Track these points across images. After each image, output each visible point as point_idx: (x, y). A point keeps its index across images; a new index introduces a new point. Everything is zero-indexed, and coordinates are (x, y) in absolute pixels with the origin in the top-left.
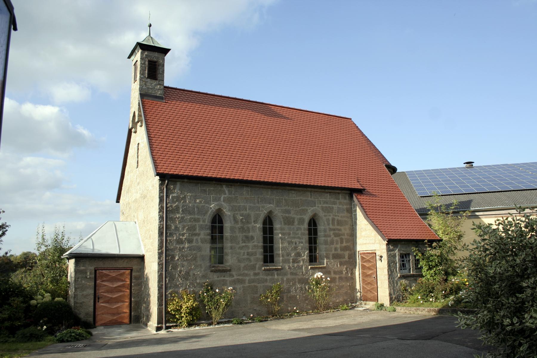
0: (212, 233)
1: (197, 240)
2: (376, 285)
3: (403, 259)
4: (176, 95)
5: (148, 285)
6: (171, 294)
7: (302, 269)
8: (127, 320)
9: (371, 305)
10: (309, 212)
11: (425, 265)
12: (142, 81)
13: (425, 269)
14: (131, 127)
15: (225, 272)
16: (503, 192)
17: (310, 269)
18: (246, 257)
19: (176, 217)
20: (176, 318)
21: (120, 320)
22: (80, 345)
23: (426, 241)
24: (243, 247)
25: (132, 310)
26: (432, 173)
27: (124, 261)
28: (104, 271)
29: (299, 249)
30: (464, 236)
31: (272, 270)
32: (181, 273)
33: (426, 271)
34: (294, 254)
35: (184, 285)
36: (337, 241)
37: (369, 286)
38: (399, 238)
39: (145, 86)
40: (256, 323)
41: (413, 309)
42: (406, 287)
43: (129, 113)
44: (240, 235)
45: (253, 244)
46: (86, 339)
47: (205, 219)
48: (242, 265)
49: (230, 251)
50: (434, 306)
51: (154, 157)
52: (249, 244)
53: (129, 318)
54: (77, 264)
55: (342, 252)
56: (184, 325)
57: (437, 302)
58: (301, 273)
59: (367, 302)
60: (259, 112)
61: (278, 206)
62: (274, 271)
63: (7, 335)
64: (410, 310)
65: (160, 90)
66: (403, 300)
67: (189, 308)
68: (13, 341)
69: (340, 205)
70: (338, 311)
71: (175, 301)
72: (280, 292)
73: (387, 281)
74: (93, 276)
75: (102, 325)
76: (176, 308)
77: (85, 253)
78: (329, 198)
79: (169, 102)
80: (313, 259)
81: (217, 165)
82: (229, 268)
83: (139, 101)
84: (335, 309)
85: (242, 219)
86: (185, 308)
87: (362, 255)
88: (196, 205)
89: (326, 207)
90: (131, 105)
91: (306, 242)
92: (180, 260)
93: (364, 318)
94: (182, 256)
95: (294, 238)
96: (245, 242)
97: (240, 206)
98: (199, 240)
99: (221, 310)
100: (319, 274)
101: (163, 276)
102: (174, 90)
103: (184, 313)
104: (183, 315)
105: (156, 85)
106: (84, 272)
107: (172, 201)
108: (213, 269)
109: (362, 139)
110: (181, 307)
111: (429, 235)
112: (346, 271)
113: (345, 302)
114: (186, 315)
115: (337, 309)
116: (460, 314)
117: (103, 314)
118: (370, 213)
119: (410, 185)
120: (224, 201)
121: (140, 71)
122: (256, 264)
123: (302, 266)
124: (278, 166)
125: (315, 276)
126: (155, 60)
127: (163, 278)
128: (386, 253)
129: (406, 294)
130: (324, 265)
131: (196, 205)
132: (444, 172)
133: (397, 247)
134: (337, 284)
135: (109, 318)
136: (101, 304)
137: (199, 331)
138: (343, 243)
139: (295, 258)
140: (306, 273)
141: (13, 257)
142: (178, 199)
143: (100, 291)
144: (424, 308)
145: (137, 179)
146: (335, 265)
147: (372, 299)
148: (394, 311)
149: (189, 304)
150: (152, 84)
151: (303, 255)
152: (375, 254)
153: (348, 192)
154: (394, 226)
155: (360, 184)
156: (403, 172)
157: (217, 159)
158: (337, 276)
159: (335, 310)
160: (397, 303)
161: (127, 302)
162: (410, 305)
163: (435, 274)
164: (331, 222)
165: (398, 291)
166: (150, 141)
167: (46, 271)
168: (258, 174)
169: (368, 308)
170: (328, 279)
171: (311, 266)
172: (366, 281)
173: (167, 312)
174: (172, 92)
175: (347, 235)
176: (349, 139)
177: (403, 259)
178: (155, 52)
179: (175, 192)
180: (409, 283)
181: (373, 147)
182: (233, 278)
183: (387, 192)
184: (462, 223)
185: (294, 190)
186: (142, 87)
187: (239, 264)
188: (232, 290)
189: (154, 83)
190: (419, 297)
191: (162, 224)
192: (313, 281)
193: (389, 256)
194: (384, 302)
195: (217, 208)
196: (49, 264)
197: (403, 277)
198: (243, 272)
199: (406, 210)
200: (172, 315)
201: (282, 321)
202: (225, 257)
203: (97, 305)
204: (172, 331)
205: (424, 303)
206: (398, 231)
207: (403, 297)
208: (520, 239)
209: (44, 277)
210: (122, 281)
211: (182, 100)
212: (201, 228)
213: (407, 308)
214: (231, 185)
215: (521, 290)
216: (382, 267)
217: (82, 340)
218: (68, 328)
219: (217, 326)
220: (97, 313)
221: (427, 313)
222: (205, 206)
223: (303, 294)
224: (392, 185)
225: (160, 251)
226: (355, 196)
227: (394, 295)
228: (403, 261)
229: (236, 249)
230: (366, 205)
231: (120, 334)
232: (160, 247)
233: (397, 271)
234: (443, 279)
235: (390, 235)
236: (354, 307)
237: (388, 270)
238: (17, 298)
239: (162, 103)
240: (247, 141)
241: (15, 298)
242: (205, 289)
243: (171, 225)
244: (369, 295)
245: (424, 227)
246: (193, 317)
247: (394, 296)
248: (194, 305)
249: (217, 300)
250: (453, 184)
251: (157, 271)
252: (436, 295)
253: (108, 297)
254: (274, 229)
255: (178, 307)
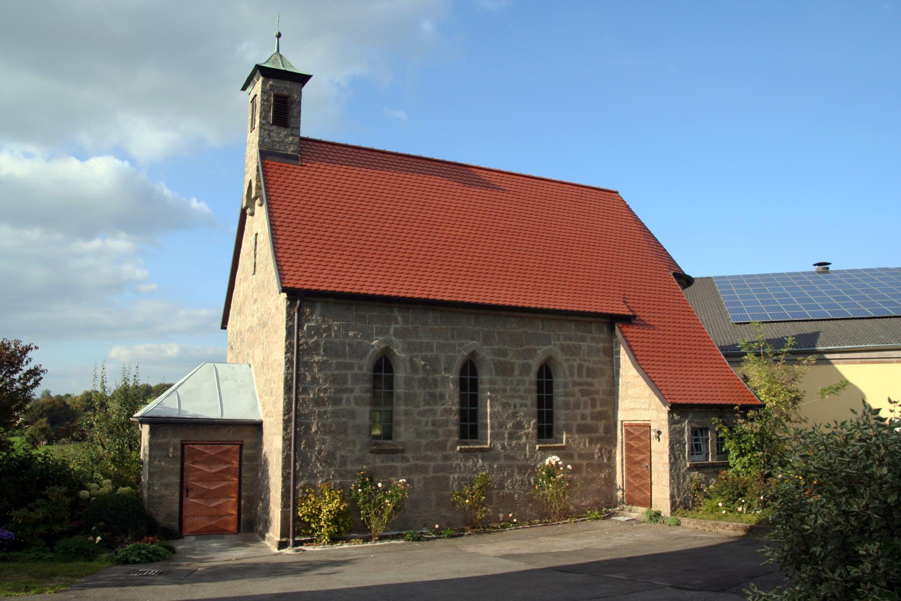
0: (374, 388)
1: (348, 400)
2: (649, 480)
3: (696, 437)
4: (320, 152)
5: (267, 471)
6: (304, 488)
7: (525, 450)
8: (233, 527)
9: (639, 512)
10: (538, 354)
11: (734, 448)
12: (264, 129)
13: (733, 454)
14: (244, 205)
15: (394, 453)
16: (877, 319)
17: (539, 450)
18: (429, 428)
19: (314, 362)
20: (312, 528)
21: (222, 527)
22: (151, 570)
23: (737, 407)
24: (426, 411)
25: (242, 510)
26: (757, 280)
27: (229, 431)
28: (197, 447)
29: (520, 416)
30: (804, 398)
31: (474, 452)
32: (321, 453)
33: (735, 458)
34: (511, 424)
35: (326, 474)
36: (586, 403)
37: (638, 481)
38: (690, 402)
39: (268, 137)
40: (443, 540)
41: (709, 523)
42: (700, 484)
43: (244, 182)
44: (421, 393)
45: (443, 407)
46: (165, 559)
47: (363, 365)
48: (424, 442)
49: (403, 418)
50: (745, 520)
51: (279, 259)
52: (436, 408)
53: (236, 523)
54: (152, 432)
55: (594, 422)
56: (324, 540)
57: (750, 513)
58: (523, 457)
59: (634, 508)
60: (459, 181)
61: (486, 344)
62: (477, 453)
63: (41, 547)
64: (705, 526)
65: (293, 144)
66: (693, 506)
67: (333, 513)
68: (49, 558)
69: (592, 342)
70: (583, 520)
71: (311, 500)
72: (485, 488)
73: (668, 475)
74: (179, 453)
75: (192, 534)
76: (311, 512)
77: (165, 416)
78: (574, 331)
79: (308, 164)
80: (546, 431)
81: (384, 274)
82: (401, 448)
83: (258, 163)
84: (578, 518)
85: (425, 365)
86: (326, 511)
87: (628, 428)
88: (347, 341)
89: (568, 345)
90: (246, 169)
91: (532, 405)
92: (319, 433)
93: (624, 537)
94: (324, 425)
95: (513, 397)
96: (429, 404)
97: (422, 342)
98: (352, 400)
99: (385, 517)
100: (553, 459)
101: (291, 459)
102: (318, 145)
103: (325, 521)
104: (322, 523)
105: (286, 136)
106: (165, 447)
107: (308, 334)
108: (375, 447)
109: (635, 228)
110: (320, 510)
111: (743, 396)
112: (599, 454)
113: (597, 506)
114: (328, 523)
115: (582, 517)
116: (753, 587)
117: (194, 516)
118: (642, 357)
119: (719, 301)
120: (395, 334)
121: (260, 112)
122: (447, 441)
123: (525, 445)
124: (500, 261)
125: (547, 462)
126: (286, 93)
127: (290, 462)
128: (667, 426)
129: (700, 497)
130: (562, 442)
131: (347, 341)
132: (778, 279)
133: (686, 417)
134: (584, 475)
135: (202, 522)
136: (192, 500)
137: (348, 551)
138: (595, 407)
139: (514, 431)
140: (532, 456)
141: (69, 398)
142: (317, 330)
143: (191, 479)
144: (727, 523)
145: (253, 293)
146: (581, 444)
147: (641, 502)
148: (678, 524)
149: (332, 506)
150: (280, 134)
151: (526, 426)
152: (648, 428)
153: (606, 320)
154: (682, 380)
155: (628, 307)
156: (710, 278)
157: (385, 263)
158: (584, 463)
159: (579, 520)
160: (684, 512)
161: (233, 498)
162: (704, 516)
163: (751, 464)
164: (576, 371)
165: (685, 492)
166: (274, 232)
167: (107, 440)
168: (454, 289)
169: (634, 518)
170: (569, 467)
171: (541, 445)
172: (633, 472)
173: (297, 519)
174: (313, 147)
175: (604, 393)
176: (612, 228)
177: (696, 437)
178: (285, 81)
179: (313, 320)
180: (705, 477)
181: (654, 241)
182: (408, 464)
183: (673, 321)
184: (801, 377)
185: (514, 317)
186: (264, 139)
187: (418, 440)
188: (404, 484)
189: (284, 132)
190: (720, 505)
191: (290, 373)
192: (542, 470)
193: (672, 432)
194: (661, 509)
195: (383, 346)
196: (113, 427)
197: (695, 467)
198: (425, 453)
199: (706, 352)
200: (305, 523)
201: (487, 536)
202: (396, 429)
203: (184, 501)
204: (304, 550)
205: (729, 514)
206: (689, 389)
207: (693, 501)
208: (863, 464)
209: (106, 449)
210: (226, 463)
211: (329, 161)
212: (356, 379)
213: (700, 521)
214: (408, 308)
215: (856, 560)
216: (660, 450)
217: (158, 560)
218: (136, 541)
219: (378, 544)
220: (184, 515)
221: (732, 532)
222: (362, 342)
223: (525, 491)
224: (683, 309)
225: (287, 417)
226: (618, 327)
227: (678, 498)
228: (696, 440)
229: (414, 415)
230: (637, 344)
231: (220, 550)
232: (287, 411)
233: (684, 457)
234: (762, 475)
235: (674, 397)
236: (610, 515)
237: (670, 455)
238: (58, 486)
239: (296, 166)
240: (438, 231)
241: (55, 488)
242: (360, 481)
243: (305, 375)
244: (637, 496)
245: (734, 382)
246: (339, 528)
247: (678, 500)
248: (342, 508)
249: (380, 499)
250: (793, 301)
251: (281, 451)
252: (749, 501)
253: (204, 488)
254: (479, 381)
255: (315, 510)
